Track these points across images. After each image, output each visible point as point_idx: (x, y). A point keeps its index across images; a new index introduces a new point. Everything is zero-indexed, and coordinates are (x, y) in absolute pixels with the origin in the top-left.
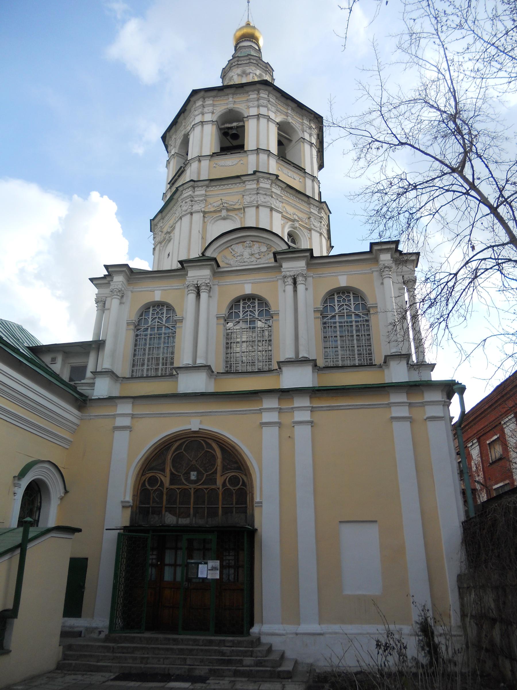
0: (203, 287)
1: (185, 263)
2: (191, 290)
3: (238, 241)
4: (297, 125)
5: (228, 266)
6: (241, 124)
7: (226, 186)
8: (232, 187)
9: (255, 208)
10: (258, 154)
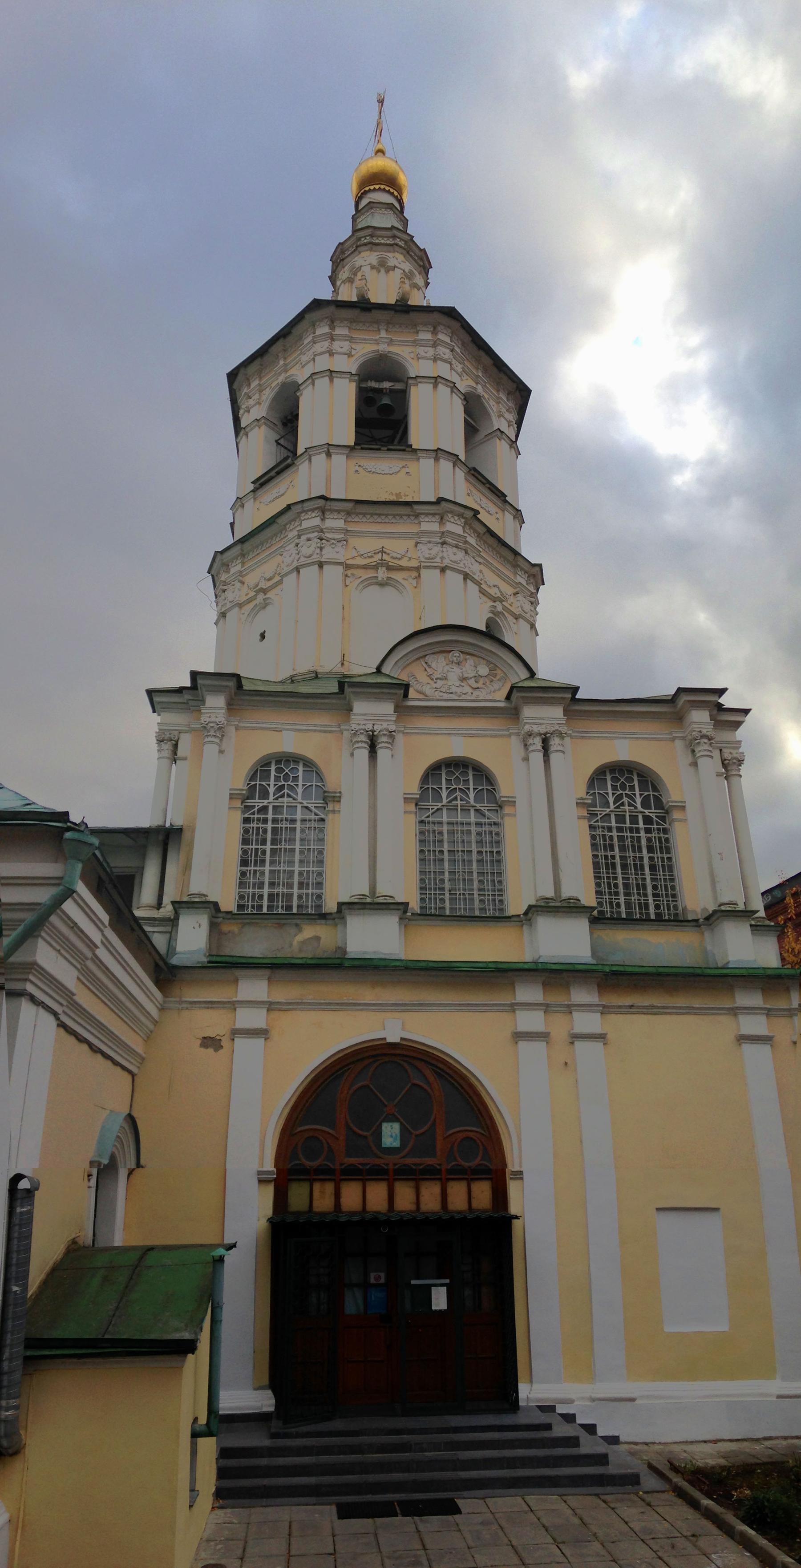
0: (384, 739)
1: (349, 686)
2: (362, 742)
3: (437, 650)
4: (492, 403)
5: (421, 697)
6: (399, 386)
7: (383, 517)
8: (394, 521)
9: (438, 571)
10: (437, 459)
